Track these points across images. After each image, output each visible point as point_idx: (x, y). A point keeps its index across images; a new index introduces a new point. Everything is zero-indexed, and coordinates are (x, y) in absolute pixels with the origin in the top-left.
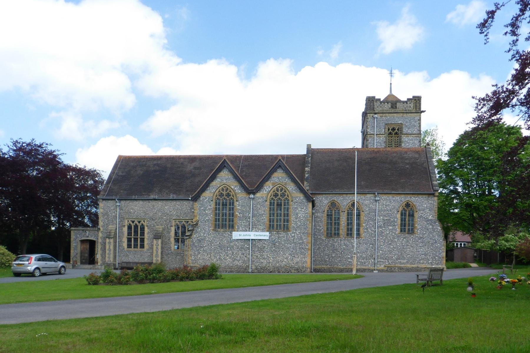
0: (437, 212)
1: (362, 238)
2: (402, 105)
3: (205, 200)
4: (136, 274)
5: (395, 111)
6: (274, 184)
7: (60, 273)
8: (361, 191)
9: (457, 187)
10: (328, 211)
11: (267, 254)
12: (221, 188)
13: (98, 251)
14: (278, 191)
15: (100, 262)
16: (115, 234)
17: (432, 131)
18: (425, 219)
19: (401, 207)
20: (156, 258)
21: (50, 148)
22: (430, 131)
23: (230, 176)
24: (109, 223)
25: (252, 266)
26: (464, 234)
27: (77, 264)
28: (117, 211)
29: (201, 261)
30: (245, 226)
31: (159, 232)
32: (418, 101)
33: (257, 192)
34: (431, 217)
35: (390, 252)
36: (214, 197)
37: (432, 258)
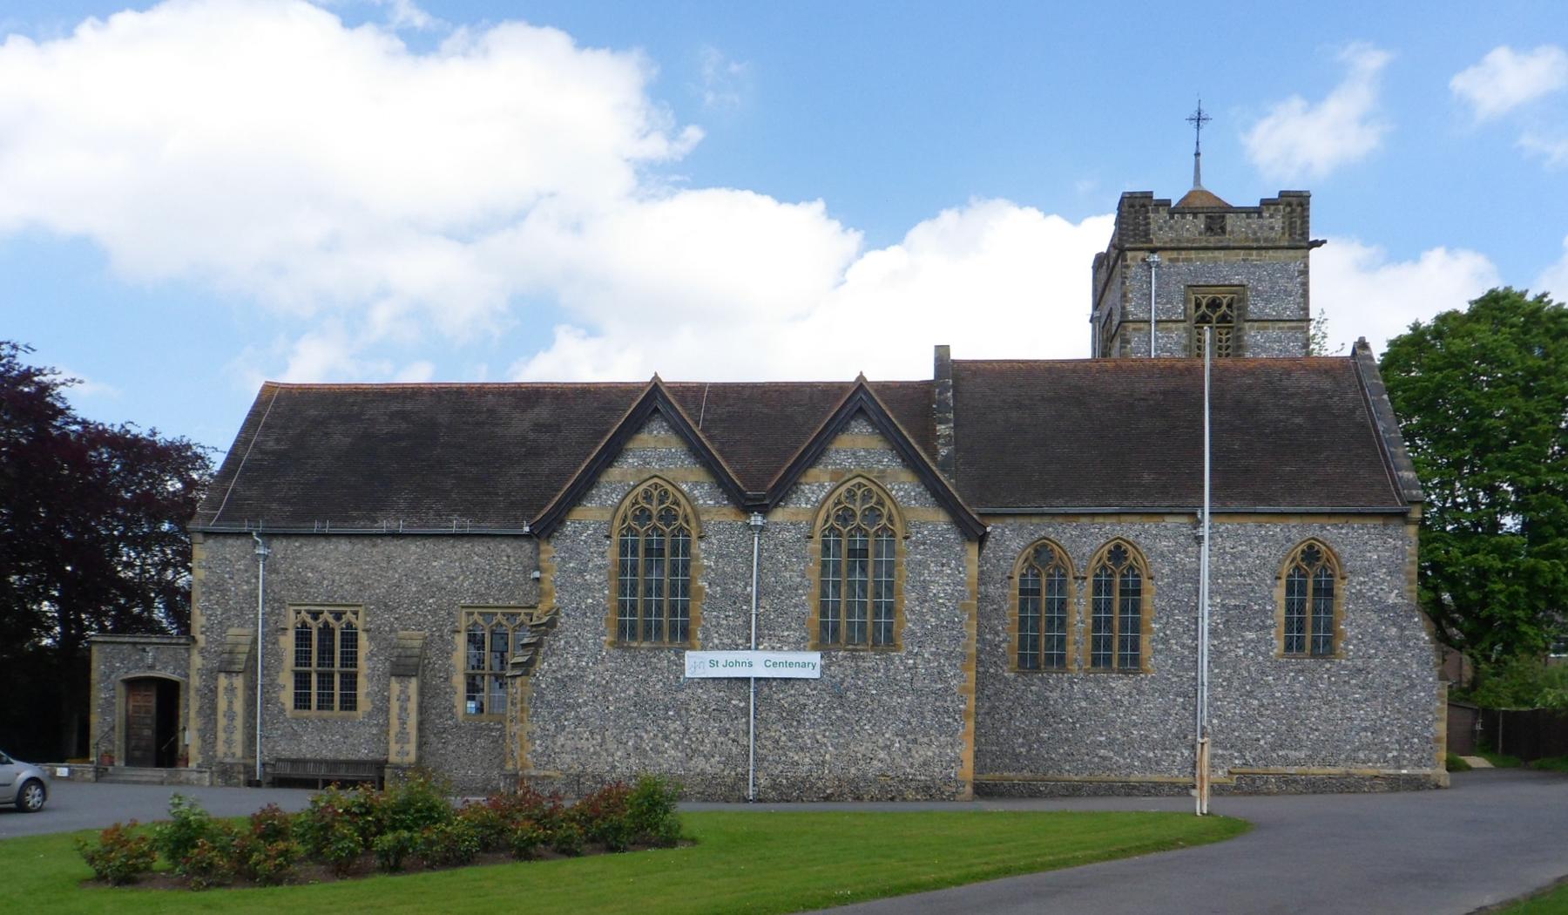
2: (1243, 224)
3: (581, 535)
4: (322, 828)
5: (1221, 242)
6: (838, 477)
7: (20, 807)
8: (1146, 504)
10: (1097, 575)
11: (814, 734)
12: (641, 489)
13: (187, 720)
15: (195, 758)
16: (252, 657)
19: (1288, 562)
23: (676, 447)
25: (760, 775)
27: (112, 764)
28: (257, 577)
29: (567, 758)
31: (409, 653)
32: (1299, 209)
33: (777, 505)
34: (1393, 595)
35: (1251, 722)
36: (617, 523)
37: (1398, 742)
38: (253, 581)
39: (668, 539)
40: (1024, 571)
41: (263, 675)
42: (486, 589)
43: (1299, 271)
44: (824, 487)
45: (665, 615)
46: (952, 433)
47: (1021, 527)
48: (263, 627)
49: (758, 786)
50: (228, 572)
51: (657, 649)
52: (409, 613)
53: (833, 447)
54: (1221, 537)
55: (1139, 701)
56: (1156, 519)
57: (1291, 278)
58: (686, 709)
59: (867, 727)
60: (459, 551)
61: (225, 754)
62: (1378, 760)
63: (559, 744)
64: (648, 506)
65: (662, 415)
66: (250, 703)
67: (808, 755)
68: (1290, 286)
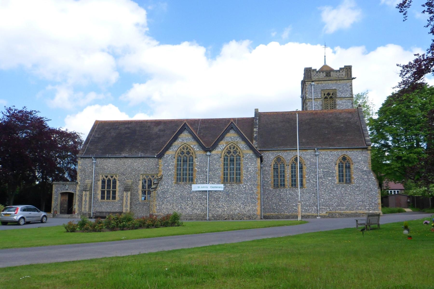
1: (305, 188)
5: (330, 78)
6: (227, 143)
7: (42, 222)
9: (388, 142)
10: (274, 165)
11: (222, 204)
12: (182, 146)
14: (231, 149)
15: (77, 212)
19: (338, 160)
21: (39, 115)
23: (190, 137)
24: (86, 178)
25: (210, 214)
28: (93, 168)
29: (165, 210)
30: (203, 179)
31: (128, 185)
32: (349, 70)
33: (213, 150)
34: (365, 168)
35: (331, 200)
36: (176, 154)
37: (369, 204)
39: (188, 158)
43: (350, 85)
44: (224, 145)
46: (257, 131)
47: (273, 153)
48: (94, 179)
49: (209, 216)
50: (86, 167)
51: (185, 184)
53: (226, 136)
55: (303, 195)
56: (305, 151)
57: (348, 87)
60: (140, 161)
64: (183, 151)
66: (90, 198)
68: (348, 89)
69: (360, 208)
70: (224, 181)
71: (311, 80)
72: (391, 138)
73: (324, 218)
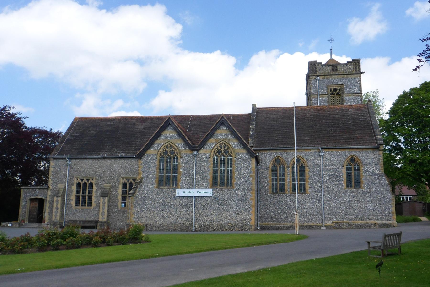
0: (383, 165)
1: (308, 193)
6: (217, 141)
9: (399, 144)
10: (272, 166)
11: (211, 212)
12: (165, 145)
13: (46, 209)
14: (221, 148)
16: (64, 192)
17: (373, 93)
18: (371, 173)
19: (346, 162)
20: (102, 216)
21: (12, 111)
22: (371, 93)
23: (175, 134)
24: (58, 181)
25: (196, 223)
26: (410, 188)
27: (24, 222)
28: (67, 170)
29: (144, 219)
30: (189, 183)
31: (106, 190)
32: (358, 64)
33: (201, 149)
34: (377, 171)
35: (338, 208)
36: (159, 154)
37: (381, 213)
38: (66, 171)
40: (273, 165)
41: (67, 197)
42: (128, 172)
44: (214, 144)
45: (171, 179)
46: (254, 128)
48: (68, 183)
50: (59, 169)
51: (168, 188)
52: (107, 179)
53: (216, 133)
54: (327, 155)
55: (306, 202)
56: (308, 150)
58: (176, 205)
59: (225, 210)
61: (55, 219)
62: (376, 219)
63: (142, 215)
64: (167, 150)
65: (171, 126)
66: (63, 205)
67: (209, 218)
69: (371, 217)
70: (213, 184)
71: (315, 75)
72: (403, 140)
73: (330, 229)
